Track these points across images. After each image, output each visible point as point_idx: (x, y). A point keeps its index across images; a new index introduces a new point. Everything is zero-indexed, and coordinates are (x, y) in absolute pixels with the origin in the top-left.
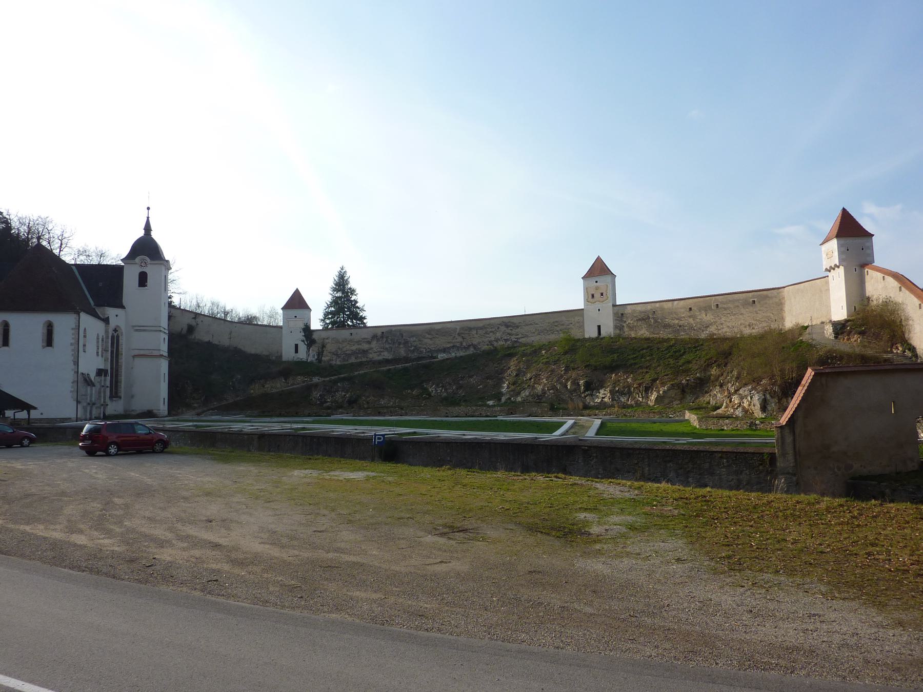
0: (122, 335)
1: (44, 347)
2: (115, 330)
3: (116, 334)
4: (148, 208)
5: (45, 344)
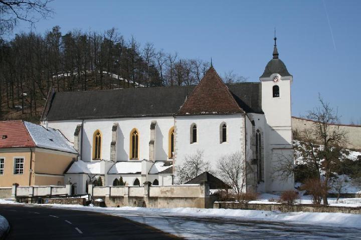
0: (263, 134)
1: (221, 143)
2: (258, 131)
3: (258, 134)
4: (275, 39)
5: (222, 140)
